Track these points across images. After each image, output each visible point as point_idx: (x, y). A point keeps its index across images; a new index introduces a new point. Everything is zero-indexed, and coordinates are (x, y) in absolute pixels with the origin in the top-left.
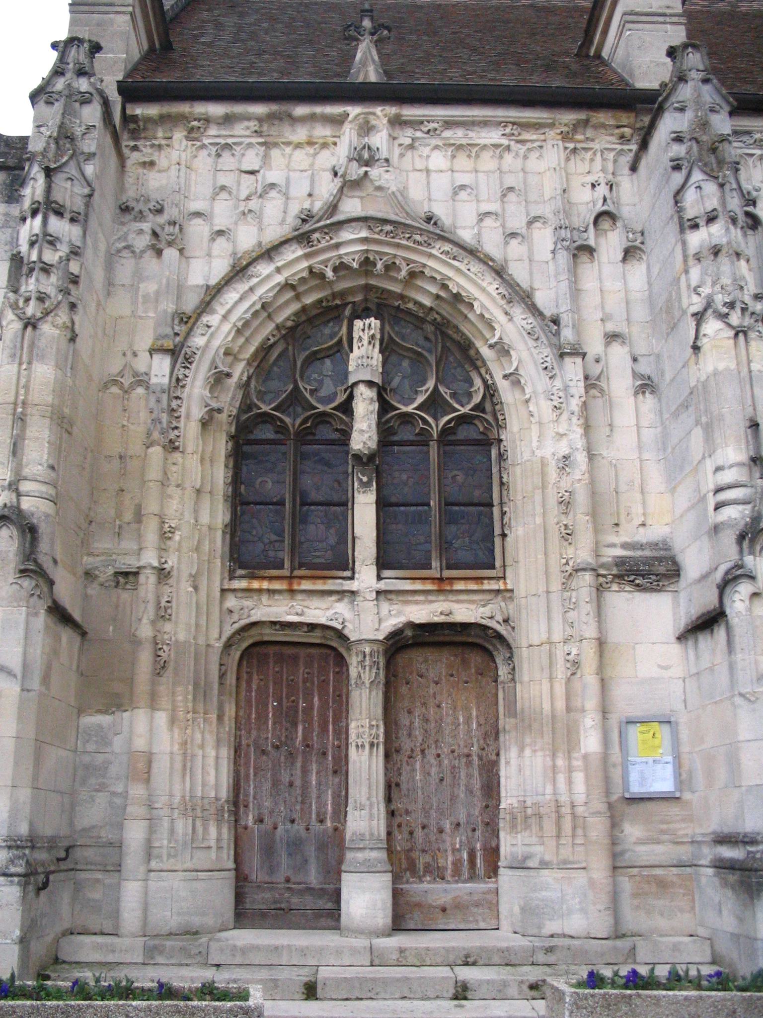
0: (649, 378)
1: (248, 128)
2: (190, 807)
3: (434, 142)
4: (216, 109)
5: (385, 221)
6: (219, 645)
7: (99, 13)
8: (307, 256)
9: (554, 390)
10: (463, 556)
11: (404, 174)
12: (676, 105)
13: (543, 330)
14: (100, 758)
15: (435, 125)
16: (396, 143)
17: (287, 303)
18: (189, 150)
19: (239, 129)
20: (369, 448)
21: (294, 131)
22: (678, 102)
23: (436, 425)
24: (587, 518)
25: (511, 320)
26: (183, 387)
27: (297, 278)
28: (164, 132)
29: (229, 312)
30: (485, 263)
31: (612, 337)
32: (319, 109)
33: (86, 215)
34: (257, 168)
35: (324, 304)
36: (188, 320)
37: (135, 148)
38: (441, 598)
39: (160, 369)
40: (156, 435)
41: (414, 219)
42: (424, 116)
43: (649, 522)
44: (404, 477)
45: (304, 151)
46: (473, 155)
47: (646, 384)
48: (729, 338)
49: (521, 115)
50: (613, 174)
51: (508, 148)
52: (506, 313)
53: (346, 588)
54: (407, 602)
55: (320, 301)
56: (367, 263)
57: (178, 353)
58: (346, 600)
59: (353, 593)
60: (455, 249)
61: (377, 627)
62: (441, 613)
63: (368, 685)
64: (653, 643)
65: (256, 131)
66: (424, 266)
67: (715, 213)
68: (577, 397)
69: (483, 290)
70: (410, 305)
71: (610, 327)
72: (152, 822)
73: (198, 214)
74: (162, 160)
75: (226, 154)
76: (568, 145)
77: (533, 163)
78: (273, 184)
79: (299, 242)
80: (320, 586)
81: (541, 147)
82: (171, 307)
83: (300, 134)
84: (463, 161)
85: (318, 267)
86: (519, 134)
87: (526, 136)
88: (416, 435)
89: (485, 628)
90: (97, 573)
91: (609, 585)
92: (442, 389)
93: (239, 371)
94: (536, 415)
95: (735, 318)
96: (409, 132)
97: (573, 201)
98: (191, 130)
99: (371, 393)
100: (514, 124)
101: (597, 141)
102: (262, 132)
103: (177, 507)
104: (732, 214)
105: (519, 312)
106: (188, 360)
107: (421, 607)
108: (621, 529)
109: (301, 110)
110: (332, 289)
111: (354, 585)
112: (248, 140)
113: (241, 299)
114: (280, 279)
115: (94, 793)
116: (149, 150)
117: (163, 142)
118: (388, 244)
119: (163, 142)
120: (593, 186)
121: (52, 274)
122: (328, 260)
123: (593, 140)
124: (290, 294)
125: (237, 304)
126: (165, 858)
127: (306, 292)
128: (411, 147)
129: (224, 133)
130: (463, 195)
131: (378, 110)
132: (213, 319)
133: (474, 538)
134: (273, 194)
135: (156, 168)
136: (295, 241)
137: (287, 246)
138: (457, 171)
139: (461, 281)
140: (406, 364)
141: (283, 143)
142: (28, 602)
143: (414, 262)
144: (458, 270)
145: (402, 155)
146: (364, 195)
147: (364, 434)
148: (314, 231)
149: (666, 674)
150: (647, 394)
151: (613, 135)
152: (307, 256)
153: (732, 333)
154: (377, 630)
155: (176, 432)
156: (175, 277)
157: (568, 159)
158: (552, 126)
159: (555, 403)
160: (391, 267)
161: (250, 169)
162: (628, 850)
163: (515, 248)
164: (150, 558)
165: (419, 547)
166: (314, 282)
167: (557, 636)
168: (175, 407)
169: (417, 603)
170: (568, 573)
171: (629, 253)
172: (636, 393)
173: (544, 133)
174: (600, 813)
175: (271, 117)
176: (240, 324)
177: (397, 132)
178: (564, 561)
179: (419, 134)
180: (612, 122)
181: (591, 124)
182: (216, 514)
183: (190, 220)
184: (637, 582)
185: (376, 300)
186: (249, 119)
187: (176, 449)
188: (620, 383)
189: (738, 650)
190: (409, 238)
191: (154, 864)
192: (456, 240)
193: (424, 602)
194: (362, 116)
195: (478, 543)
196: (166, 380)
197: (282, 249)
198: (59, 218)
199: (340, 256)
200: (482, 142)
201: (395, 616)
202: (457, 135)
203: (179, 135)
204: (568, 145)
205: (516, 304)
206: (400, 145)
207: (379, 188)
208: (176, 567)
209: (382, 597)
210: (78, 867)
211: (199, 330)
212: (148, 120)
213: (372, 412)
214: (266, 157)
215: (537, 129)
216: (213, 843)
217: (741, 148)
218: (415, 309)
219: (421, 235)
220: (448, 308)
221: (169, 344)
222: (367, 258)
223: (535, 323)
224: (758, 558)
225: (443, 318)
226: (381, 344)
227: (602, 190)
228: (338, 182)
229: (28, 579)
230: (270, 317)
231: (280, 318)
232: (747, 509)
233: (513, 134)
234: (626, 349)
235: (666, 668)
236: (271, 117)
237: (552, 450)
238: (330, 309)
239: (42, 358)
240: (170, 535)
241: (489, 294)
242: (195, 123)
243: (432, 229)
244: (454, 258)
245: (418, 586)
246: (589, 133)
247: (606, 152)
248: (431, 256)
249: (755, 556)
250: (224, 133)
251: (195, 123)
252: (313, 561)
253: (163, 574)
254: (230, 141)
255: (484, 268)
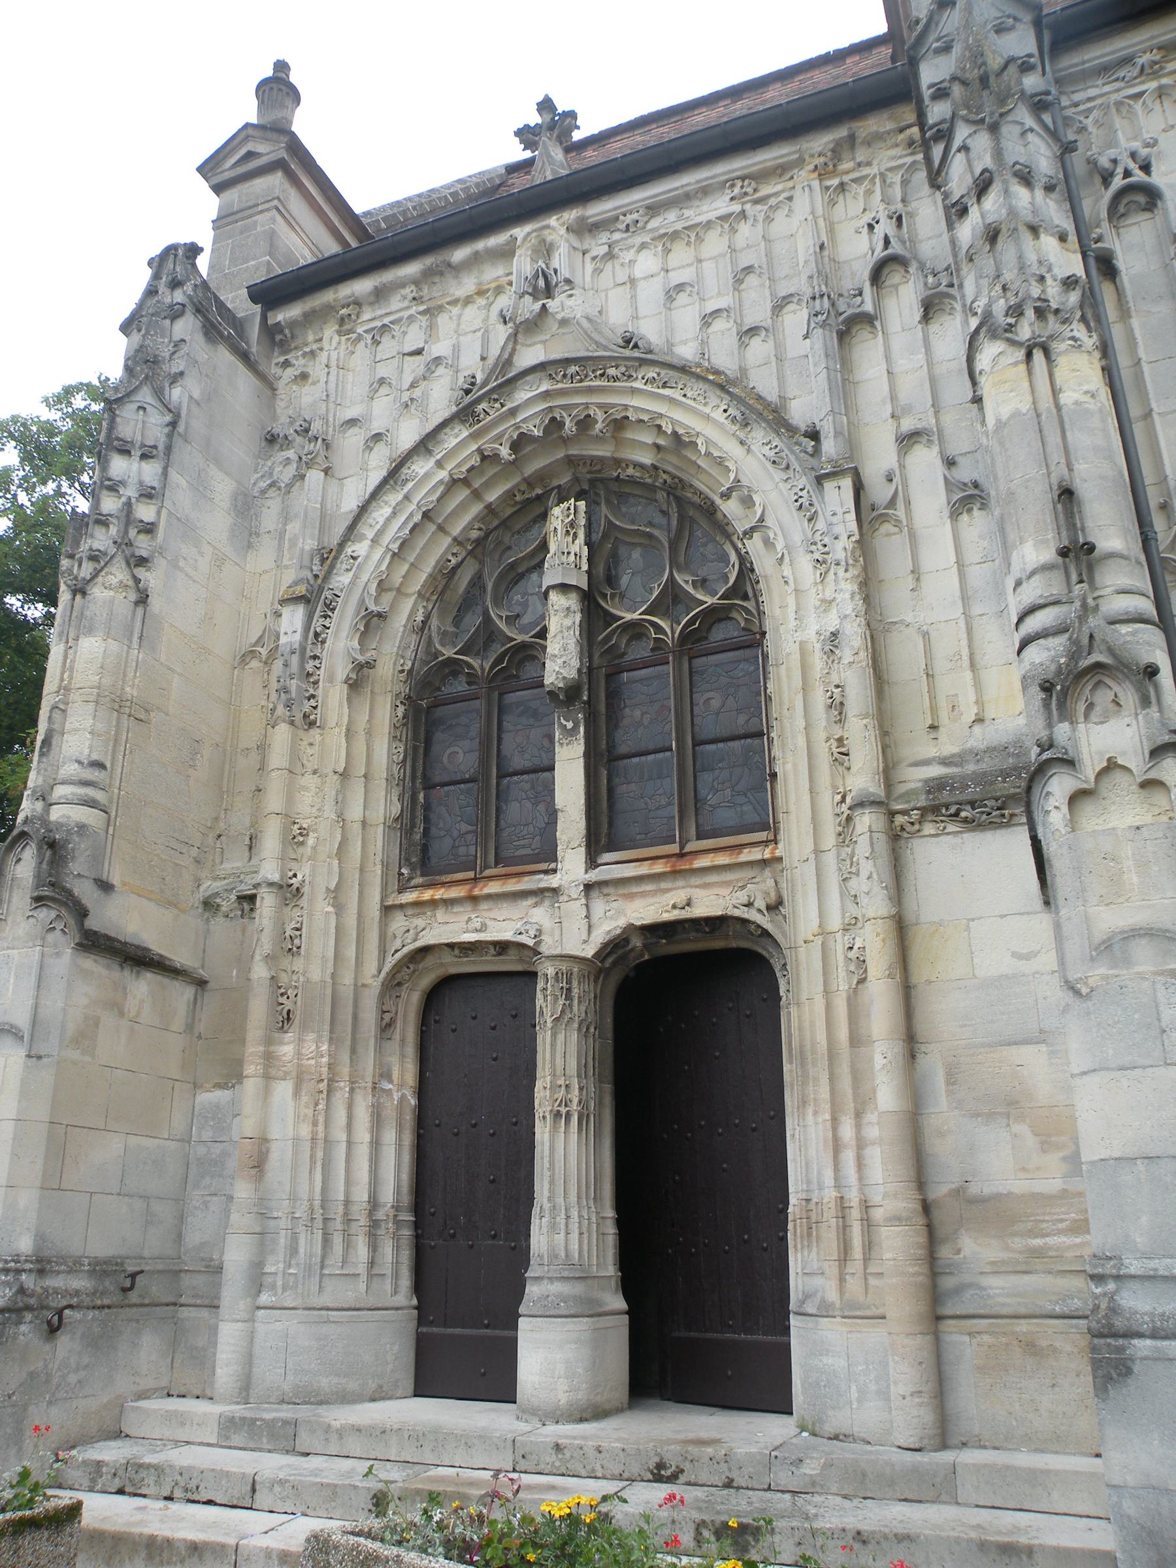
0: (976, 485)
1: (405, 298)
2: (326, 1220)
3: (638, 240)
4: (362, 286)
5: (568, 361)
6: (376, 985)
7: (243, 219)
8: (474, 436)
9: (818, 537)
10: (726, 816)
11: (603, 295)
12: (935, 45)
13: (792, 452)
14: (217, 1149)
15: (635, 216)
16: (588, 257)
17: (463, 506)
18: (343, 347)
19: (396, 303)
20: (564, 678)
21: (460, 283)
22: (938, 40)
23: (669, 629)
24: (865, 721)
25: (749, 451)
26: (323, 642)
27: (464, 469)
28: (315, 333)
29: (380, 533)
30: (705, 379)
31: (908, 440)
32: (480, 245)
33: (169, 449)
34: (421, 346)
35: (518, 498)
36: (329, 557)
37: (286, 364)
38: (680, 883)
39: (293, 620)
40: (280, 710)
41: (606, 348)
42: (615, 209)
43: (989, 714)
44: (638, 713)
45: (476, 306)
46: (693, 239)
47: (971, 496)
48: (1016, 364)
49: (750, 162)
50: (903, 201)
51: (743, 215)
52: (742, 443)
53: (542, 885)
54: (631, 897)
55: (510, 494)
56: (555, 424)
57: (314, 598)
58: (547, 903)
59: (555, 891)
60: (663, 372)
61: (585, 937)
62: (674, 907)
63: (549, 1025)
64: (1002, 916)
65: (414, 299)
66: (626, 407)
67: (987, 175)
68: (844, 537)
69: (707, 417)
70: (630, 471)
71: (908, 425)
72: (263, 1238)
73: (352, 422)
74: (316, 370)
75: (386, 340)
76: (828, 183)
77: (782, 224)
78: (438, 358)
79: (463, 422)
80: (512, 886)
81: (790, 199)
82: (310, 544)
83: (467, 285)
84: (681, 254)
85: (488, 448)
86: (755, 190)
87: (766, 190)
88: (652, 650)
89: (745, 922)
90: (218, 900)
91: (917, 827)
92: (679, 578)
93: (406, 612)
94: (791, 582)
95: (1025, 332)
96: (604, 237)
97: (842, 258)
98: (342, 321)
99: (572, 601)
100: (743, 178)
101: (875, 162)
102: (422, 297)
103: (313, 802)
104: (1018, 167)
105: (759, 436)
106: (330, 607)
107: (651, 900)
108: (943, 733)
109: (460, 254)
110: (522, 474)
111: (553, 881)
112: (406, 314)
113: (394, 513)
114: (443, 474)
115: (208, 1198)
116: (302, 361)
117: (315, 347)
118: (577, 392)
119: (315, 347)
120: (871, 227)
121: (111, 526)
122: (500, 436)
123: (869, 164)
124: (463, 494)
125: (389, 519)
126: (280, 1291)
127: (488, 485)
128: (610, 256)
129: (379, 312)
130: (682, 298)
131: (553, 221)
132: (360, 548)
133: (738, 788)
134: (441, 370)
135: (310, 381)
136: (456, 421)
137: (447, 430)
138: (674, 269)
139: (678, 415)
140: (636, 554)
141: (448, 303)
142: (43, 939)
143: (613, 406)
144: (671, 400)
145: (598, 271)
146: (547, 337)
147: (561, 660)
148: (478, 401)
149: (1026, 967)
150: (976, 512)
151: (897, 145)
152: (474, 436)
153: (1021, 354)
154: (585, 942)
155: (313, 702)
156: (318, 506)
157: (832, 203)
158: (800, 162)
159: (817, 556)
160: (585, 423)
161: (414, 348)
162: (970, 1285)
163: (758, 348)
164: (270, 871)
165: (659, 813)
166: (491, 471)
167: (835, 922)
168: (311, 670)
169: (643, 894)
170: (845, 815)
171: (930, 308)
172: (955, 515)
173: (792, 178)
174: (899, 1219)
175: (429, 275)
176: (395, 547)
177: (588, 242)
178: (838, 798)
179: (617, 236)
180: (890, 126)
181: (858, 141)
182: (378, 804)
183: (345, 432)
184: (963, 814)
185: (588, 476)
186: (403, 285)
187: (312, 724)
188: (928, 501)
189: (1061, 902)
190: (602, 375)
191: (265, 1298)
192: (675, 361)
193: (655, 893)
194: (535, 234)
195: (745, 794)
196: (298, 637)
197: (442, 436)
198: (127, 457)
199: (517, 426)
200: (703, 218)
201: (611, 918)
202: (670, 220)
203: (329, 331)
204: (828, 183)
205: (755, 425)
206: (594, 258)
207: (564, 322)
208: (307, 879)
209: (595, 893)
210: (183, 1300)
211: (341, 566)
212: (293, 324)
213: (569, 628)
214: (432, 327)
215: (780, 176)
216: (362, 1269)
217: (1118, 90)
218: (637, 474)
219: (617, 367)
220: (673, 459)
221: (301, 590)
222: (553, 419)
223: (781, 445)
224: (1081, 727)
225: (674, 477)
226: (588, 535)
227: (885, 227)
228: (509, 329)
229: (45, 909)
230: (441, 528)
231: (456, 529)
232: (1058, 644)
233: (746, 194)
234: (936, 449)
235: (1027, 957)
236: (429, 275)
237: (814, 627)
238: (528, 502)
239: (90, 631)
240: (301, 839)
241: (715, 422)
242: (344, 311)
243: (635, 355)
244: (665, 385)
245: (643, 869)
246: (861, 155)
247: (889, 174)
248: (634, 391)
249: (1073, 723)
250: (379, 312)
251: (344, 311)
252: (517, 853)
253: (289, 892)
254: (386, 321)
255: (706, 386)
